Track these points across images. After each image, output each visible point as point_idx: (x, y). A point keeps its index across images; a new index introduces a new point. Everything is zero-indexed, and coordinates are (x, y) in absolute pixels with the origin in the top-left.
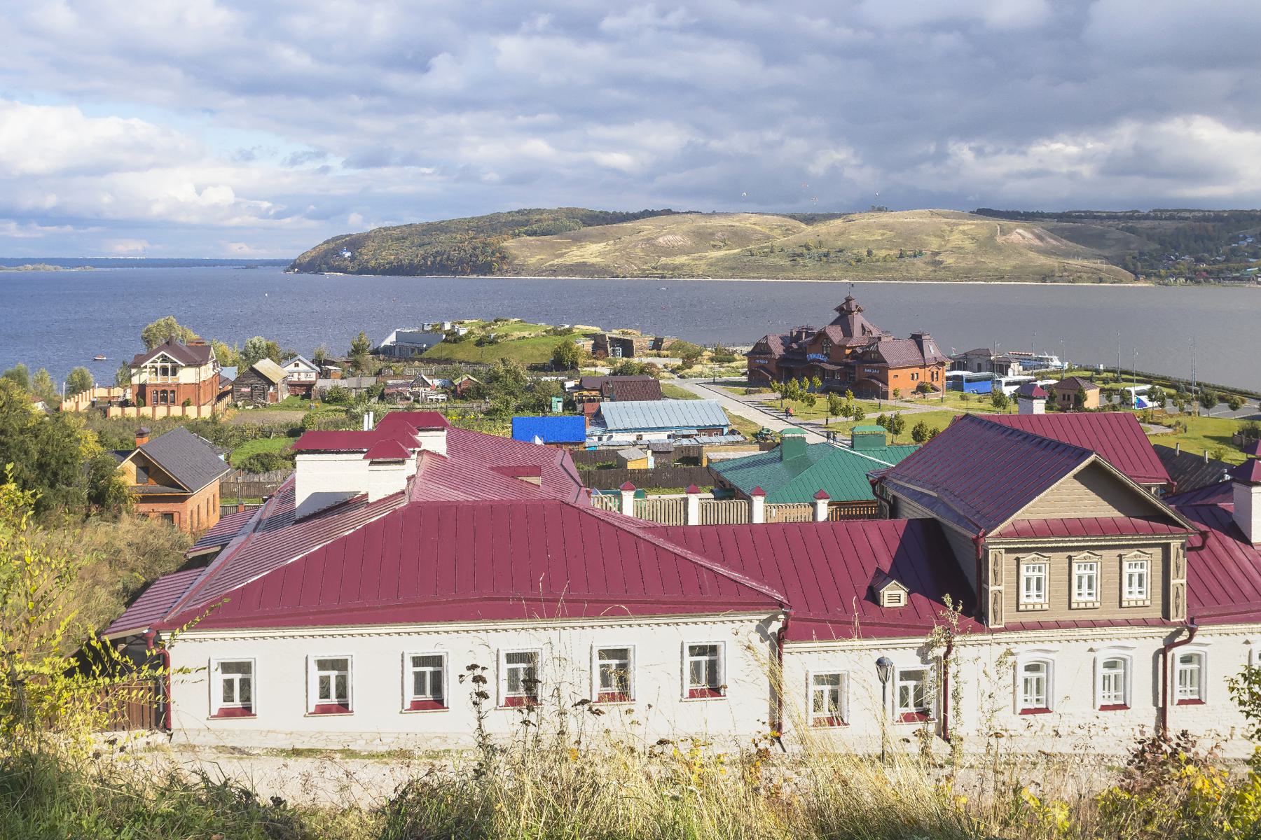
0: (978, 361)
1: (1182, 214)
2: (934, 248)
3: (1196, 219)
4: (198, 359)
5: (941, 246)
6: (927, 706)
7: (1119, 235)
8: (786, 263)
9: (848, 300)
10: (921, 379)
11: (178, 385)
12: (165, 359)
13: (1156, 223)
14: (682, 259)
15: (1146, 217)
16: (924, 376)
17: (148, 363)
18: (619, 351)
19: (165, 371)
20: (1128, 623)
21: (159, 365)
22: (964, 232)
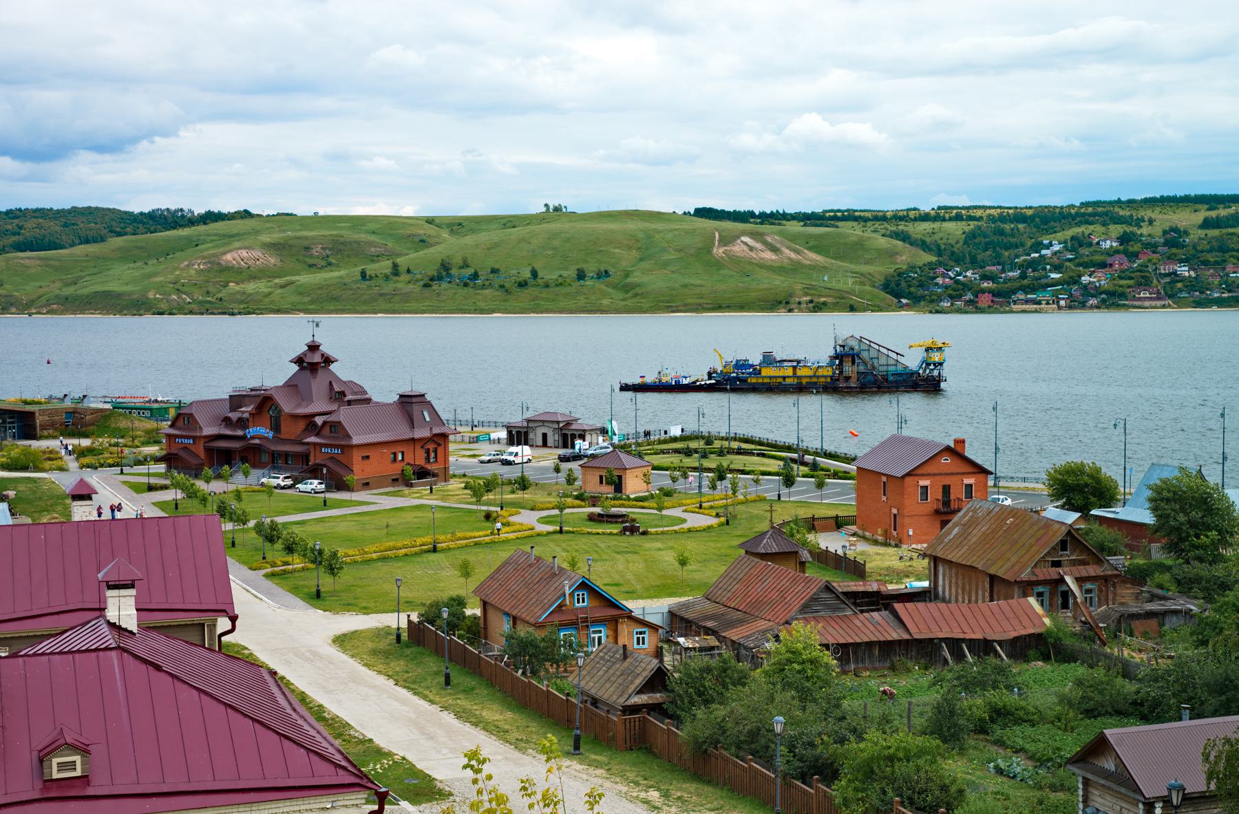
1: (972, 213)
3: (991, 219)
7: (883, 242)
8: (416, 288)
13: (937, 225)
15: (925, 217)
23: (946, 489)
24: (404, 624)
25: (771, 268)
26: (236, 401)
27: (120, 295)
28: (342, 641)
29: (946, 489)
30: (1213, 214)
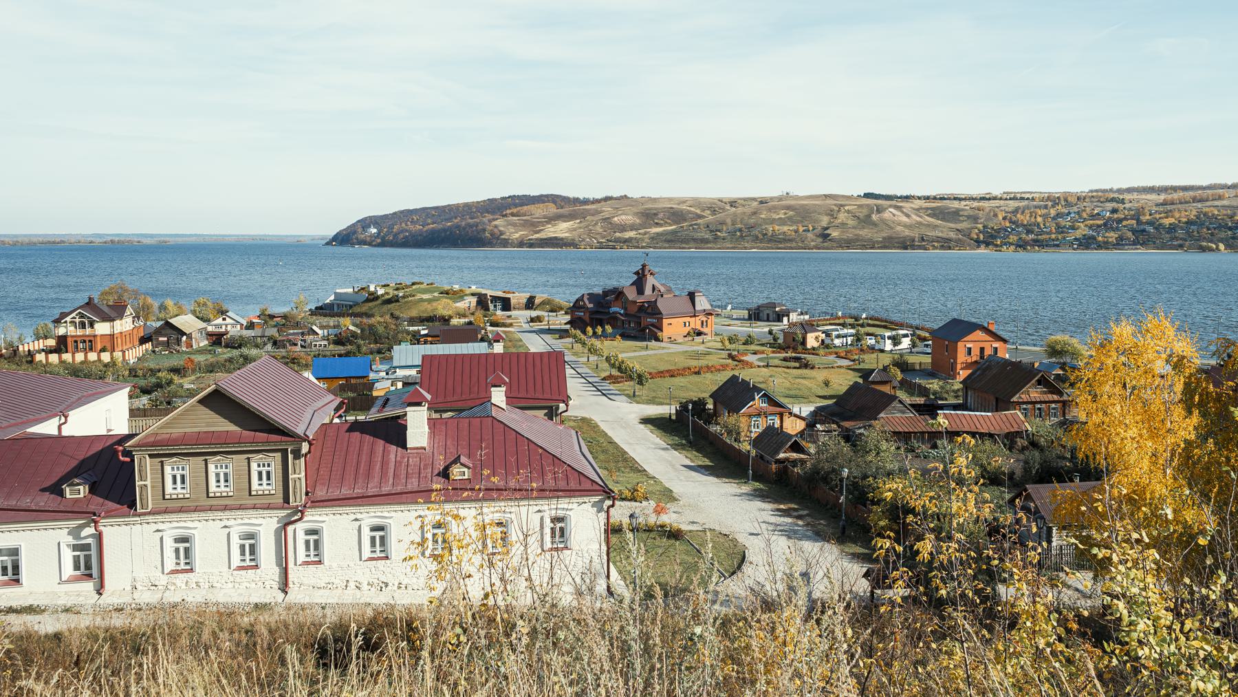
0: (766, 312)
2: (824, 224)
4: (113, 315)
5: (830, 222)
6: (90, 566)
9: (644, 266)
10: (693, 326)
11: (95, 336)
12: (82, 316)
14: (632, 234)
16: (696, 323)
17: (68, 319)
18: (499, 306)
19: (83, 326)
20: (254, 507)
21: (77, 320)
22: (848, 212)
23: (982, 349)
24: (673, 411)
25: (905, 226)
26: (606, 293)
27: (562, 239)
28: (646, 421)
29: (982, 349)
30: (1170, 197)
